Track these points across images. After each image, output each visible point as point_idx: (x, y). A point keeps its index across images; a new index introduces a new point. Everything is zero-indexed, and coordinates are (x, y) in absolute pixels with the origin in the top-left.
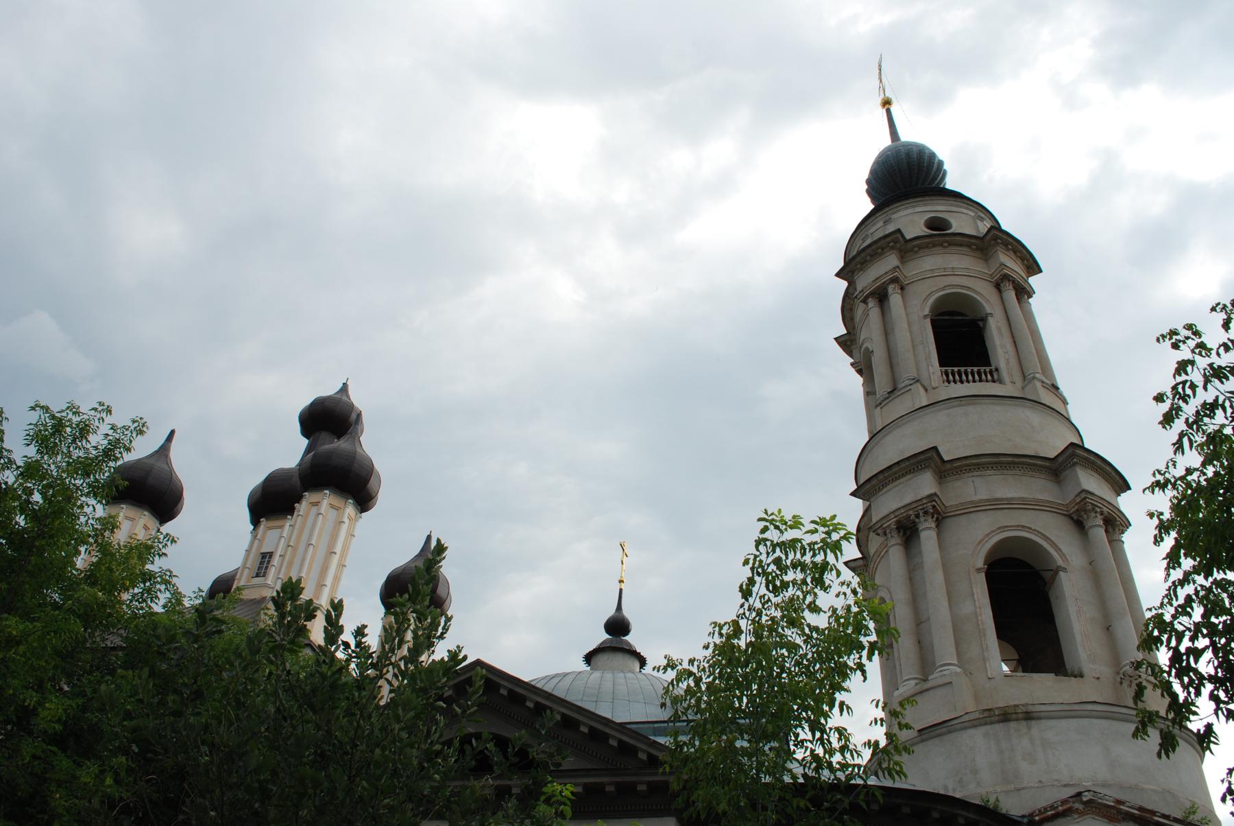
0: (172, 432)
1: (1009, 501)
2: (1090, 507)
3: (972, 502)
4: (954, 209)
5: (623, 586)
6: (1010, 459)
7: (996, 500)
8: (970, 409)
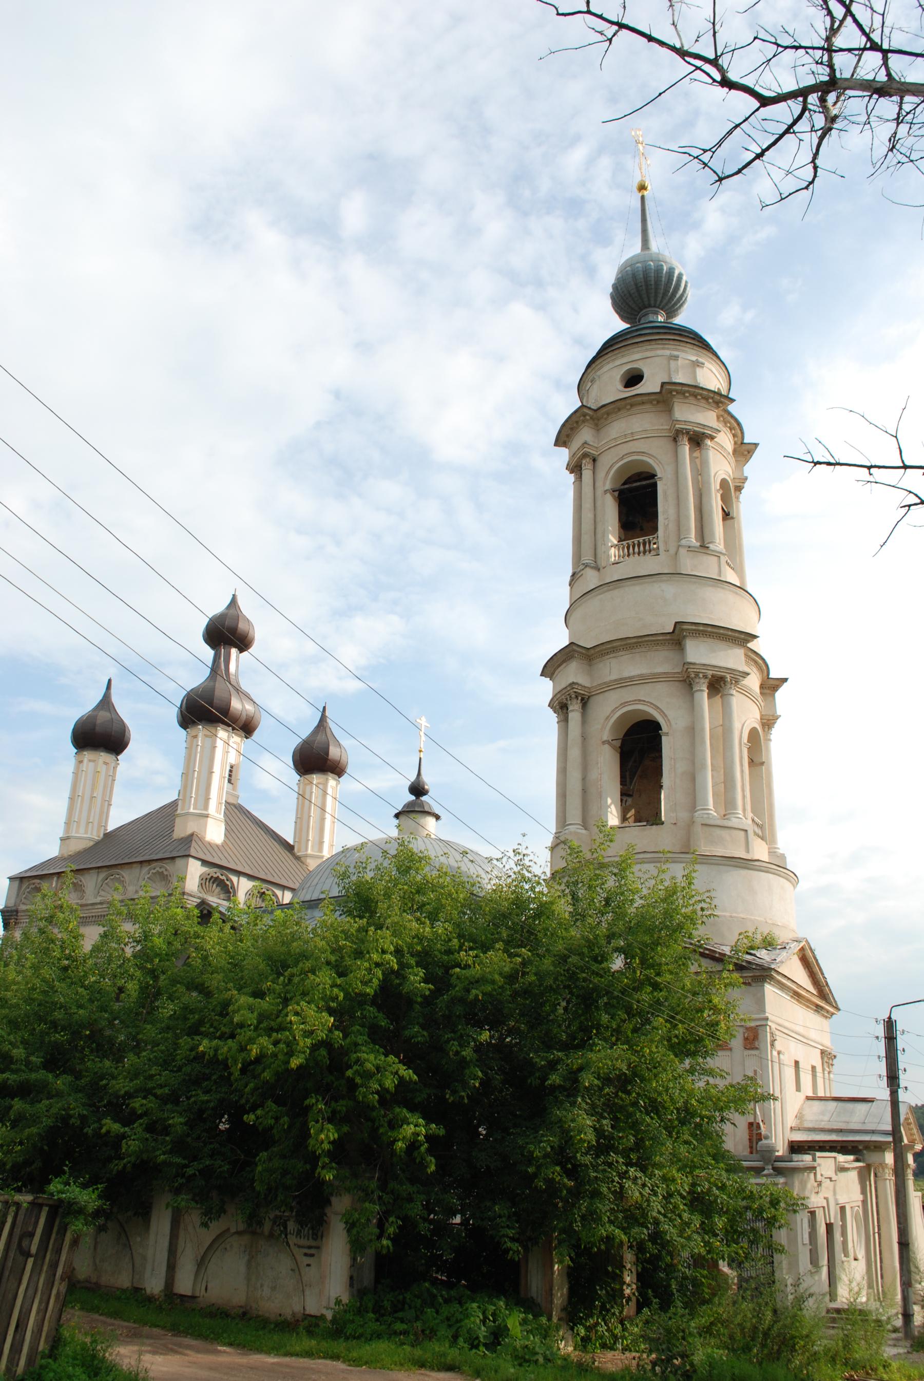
0: (110, 681)
1: (631, 679)
2: (693, 676)
3: (605, 683)
4: (648, 354)
5: (646, 193)
6: (635, 640)
7: (621, 679)
8: (616, 592)
